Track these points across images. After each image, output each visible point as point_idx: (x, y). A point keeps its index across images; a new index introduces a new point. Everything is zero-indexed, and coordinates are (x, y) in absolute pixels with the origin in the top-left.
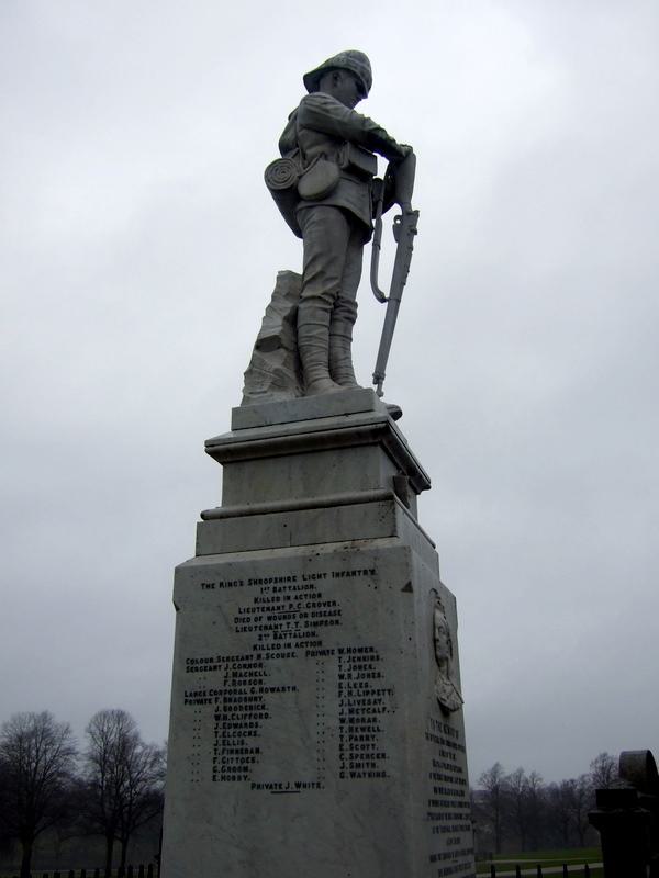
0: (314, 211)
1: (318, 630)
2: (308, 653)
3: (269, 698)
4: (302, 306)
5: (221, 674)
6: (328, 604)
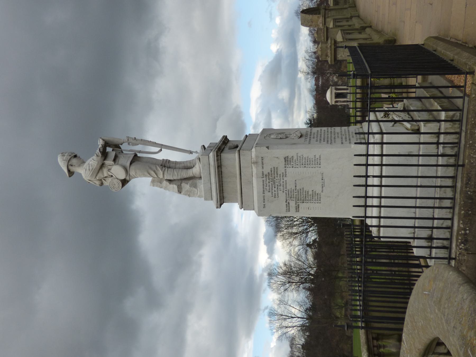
0: (131, 174)
1: (279, 173)
2: (286, 177)
3: (298, 188)
4: (165, 178)
5: (290, 202)
6: (271, 171)
